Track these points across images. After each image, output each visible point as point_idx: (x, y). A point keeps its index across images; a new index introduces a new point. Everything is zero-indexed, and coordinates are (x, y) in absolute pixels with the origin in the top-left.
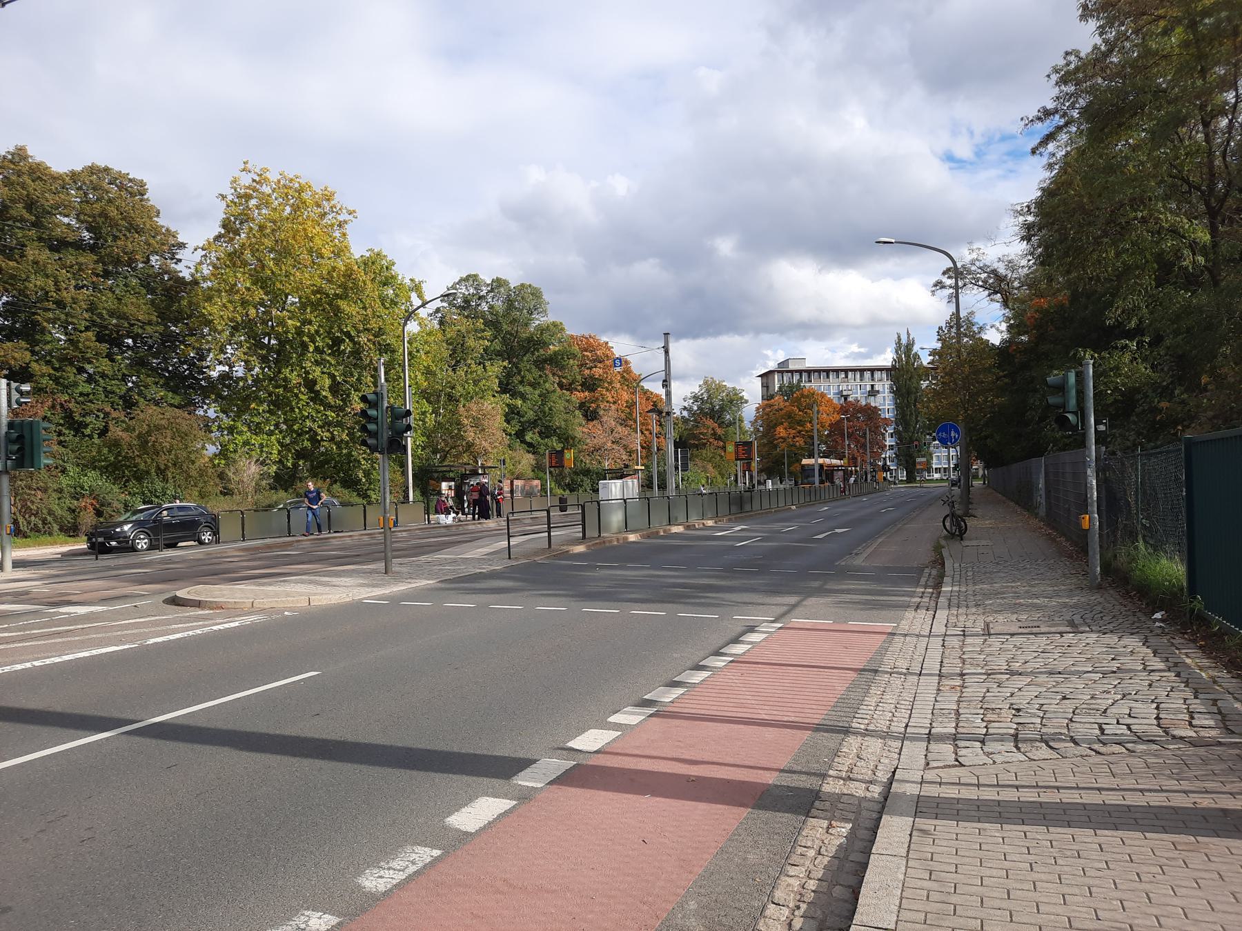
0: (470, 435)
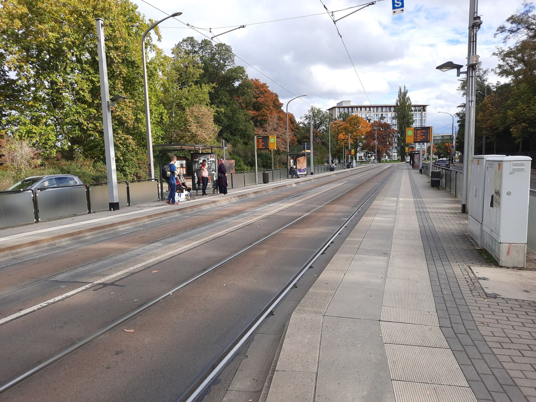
0: (194, 128)
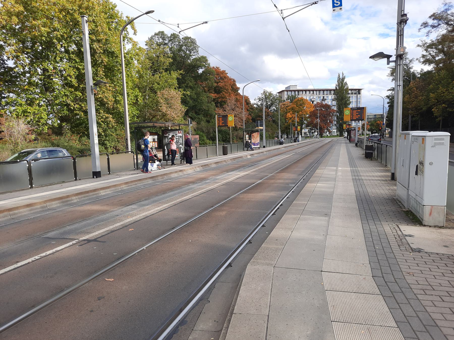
0: (164, 108)
